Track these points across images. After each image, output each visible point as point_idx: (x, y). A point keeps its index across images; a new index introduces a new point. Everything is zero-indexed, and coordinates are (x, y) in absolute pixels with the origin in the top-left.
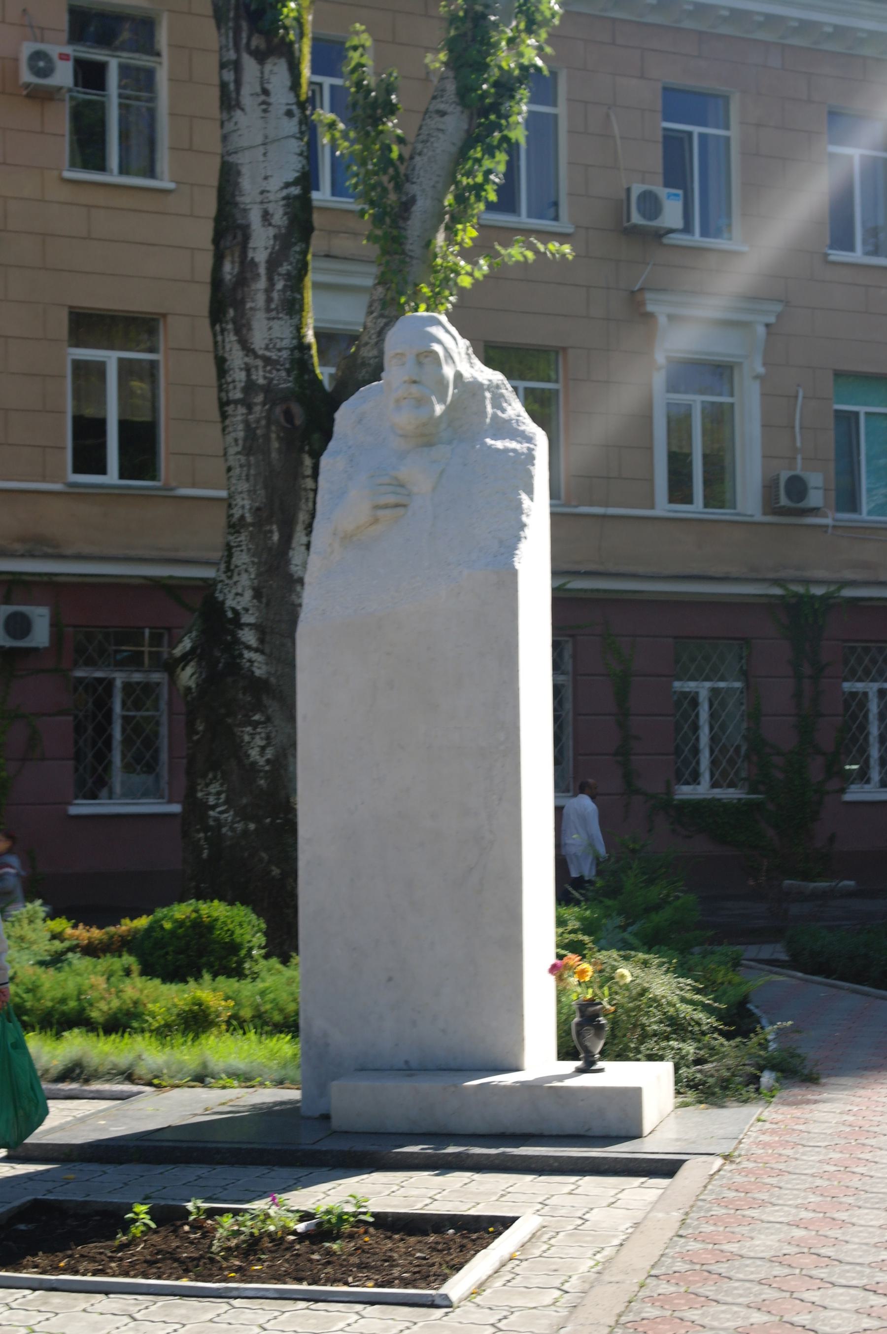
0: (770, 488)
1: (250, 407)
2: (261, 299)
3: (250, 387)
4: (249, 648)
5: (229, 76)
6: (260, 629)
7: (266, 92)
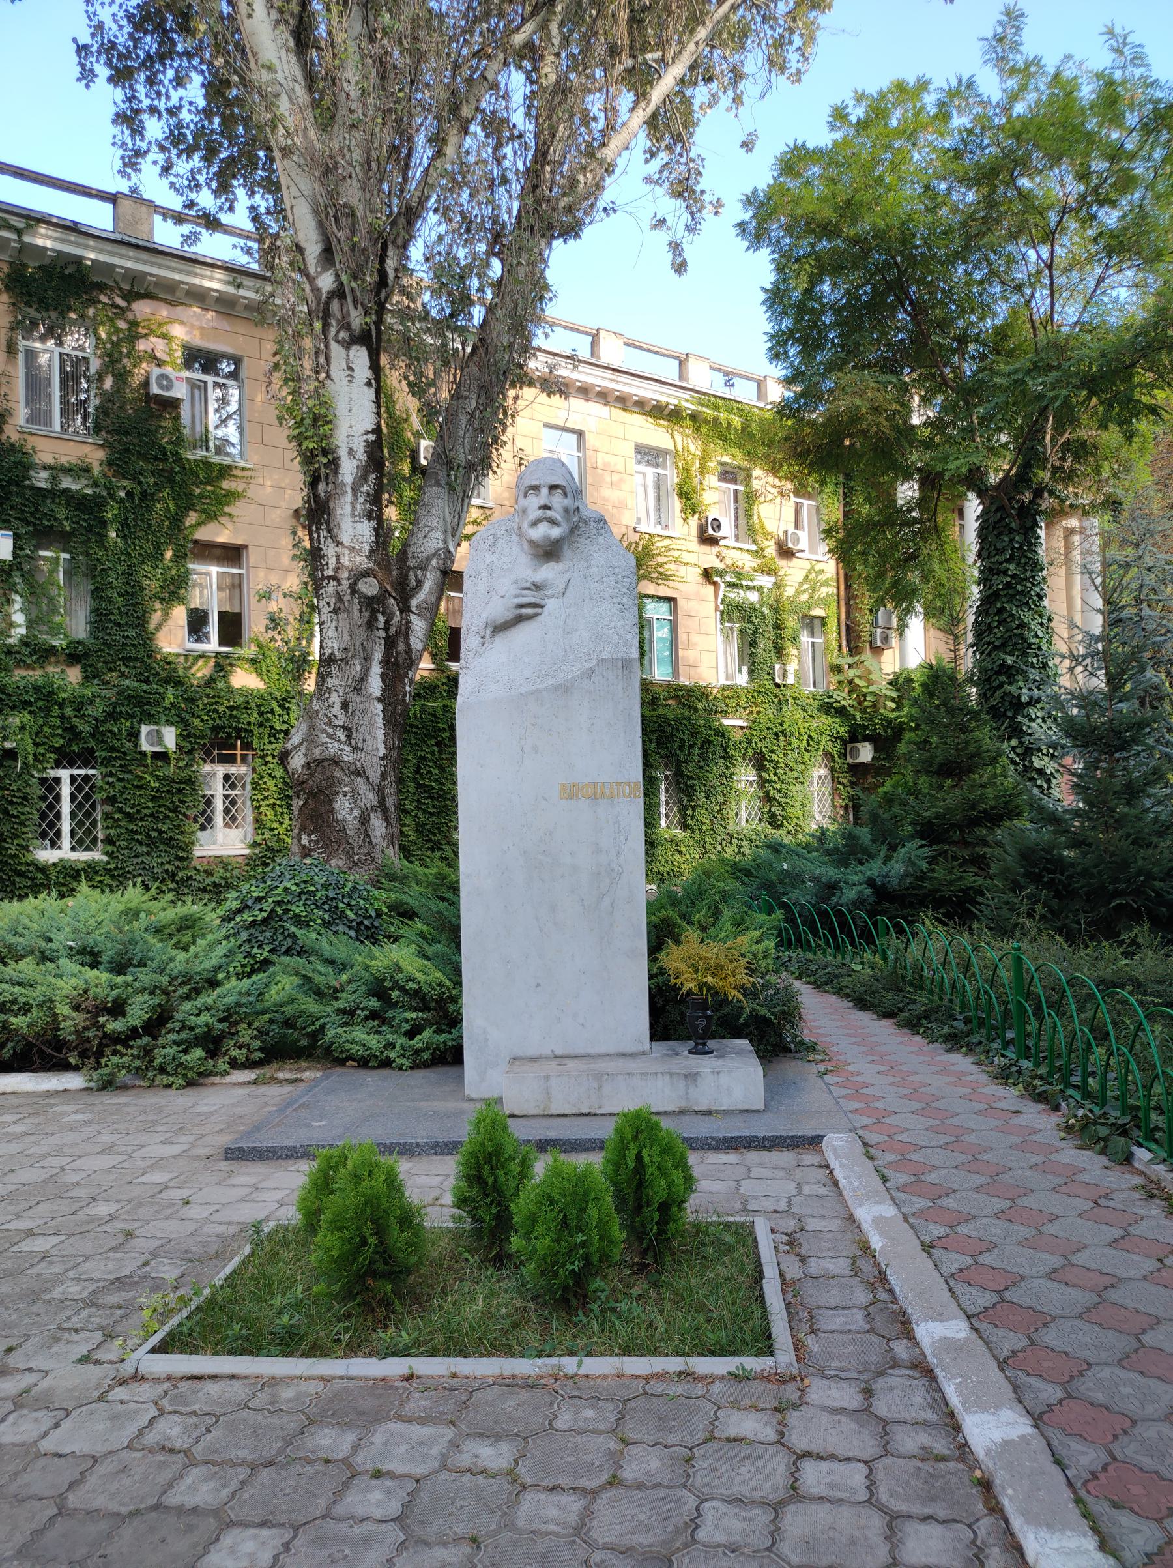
1: (338, 582)
7: (350, 368)
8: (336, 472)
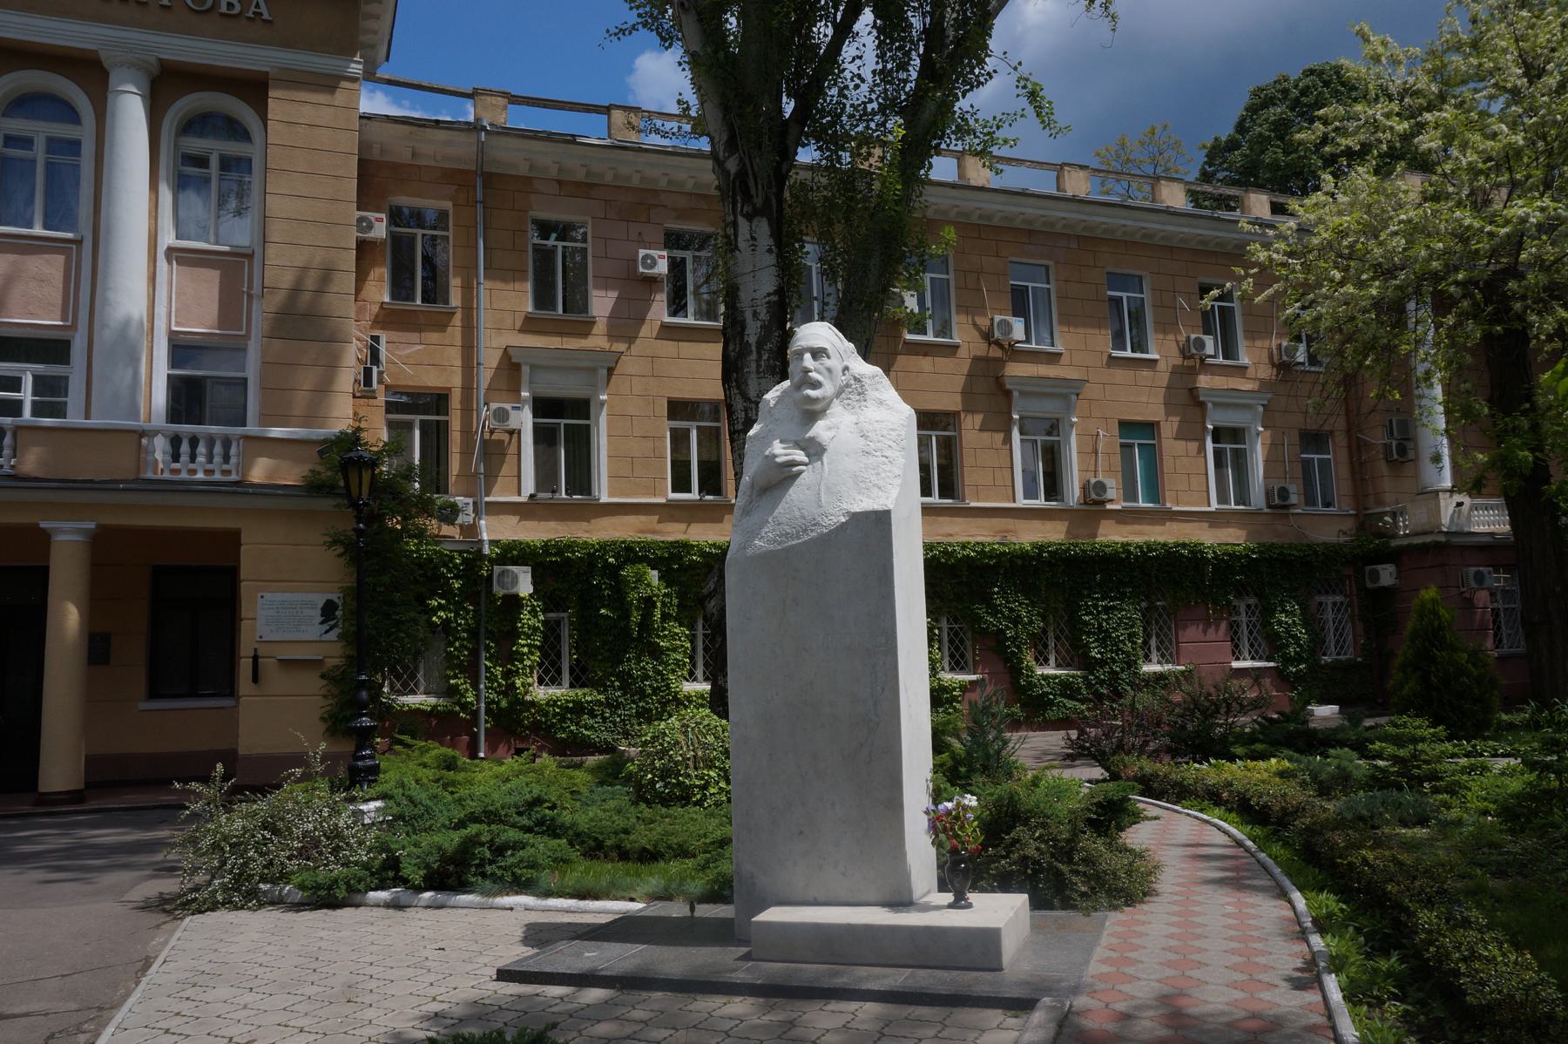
0: (1268, 494)
2: (753, 366)
5: (730, 231)
7: (753, 238)
8: (742, 333)
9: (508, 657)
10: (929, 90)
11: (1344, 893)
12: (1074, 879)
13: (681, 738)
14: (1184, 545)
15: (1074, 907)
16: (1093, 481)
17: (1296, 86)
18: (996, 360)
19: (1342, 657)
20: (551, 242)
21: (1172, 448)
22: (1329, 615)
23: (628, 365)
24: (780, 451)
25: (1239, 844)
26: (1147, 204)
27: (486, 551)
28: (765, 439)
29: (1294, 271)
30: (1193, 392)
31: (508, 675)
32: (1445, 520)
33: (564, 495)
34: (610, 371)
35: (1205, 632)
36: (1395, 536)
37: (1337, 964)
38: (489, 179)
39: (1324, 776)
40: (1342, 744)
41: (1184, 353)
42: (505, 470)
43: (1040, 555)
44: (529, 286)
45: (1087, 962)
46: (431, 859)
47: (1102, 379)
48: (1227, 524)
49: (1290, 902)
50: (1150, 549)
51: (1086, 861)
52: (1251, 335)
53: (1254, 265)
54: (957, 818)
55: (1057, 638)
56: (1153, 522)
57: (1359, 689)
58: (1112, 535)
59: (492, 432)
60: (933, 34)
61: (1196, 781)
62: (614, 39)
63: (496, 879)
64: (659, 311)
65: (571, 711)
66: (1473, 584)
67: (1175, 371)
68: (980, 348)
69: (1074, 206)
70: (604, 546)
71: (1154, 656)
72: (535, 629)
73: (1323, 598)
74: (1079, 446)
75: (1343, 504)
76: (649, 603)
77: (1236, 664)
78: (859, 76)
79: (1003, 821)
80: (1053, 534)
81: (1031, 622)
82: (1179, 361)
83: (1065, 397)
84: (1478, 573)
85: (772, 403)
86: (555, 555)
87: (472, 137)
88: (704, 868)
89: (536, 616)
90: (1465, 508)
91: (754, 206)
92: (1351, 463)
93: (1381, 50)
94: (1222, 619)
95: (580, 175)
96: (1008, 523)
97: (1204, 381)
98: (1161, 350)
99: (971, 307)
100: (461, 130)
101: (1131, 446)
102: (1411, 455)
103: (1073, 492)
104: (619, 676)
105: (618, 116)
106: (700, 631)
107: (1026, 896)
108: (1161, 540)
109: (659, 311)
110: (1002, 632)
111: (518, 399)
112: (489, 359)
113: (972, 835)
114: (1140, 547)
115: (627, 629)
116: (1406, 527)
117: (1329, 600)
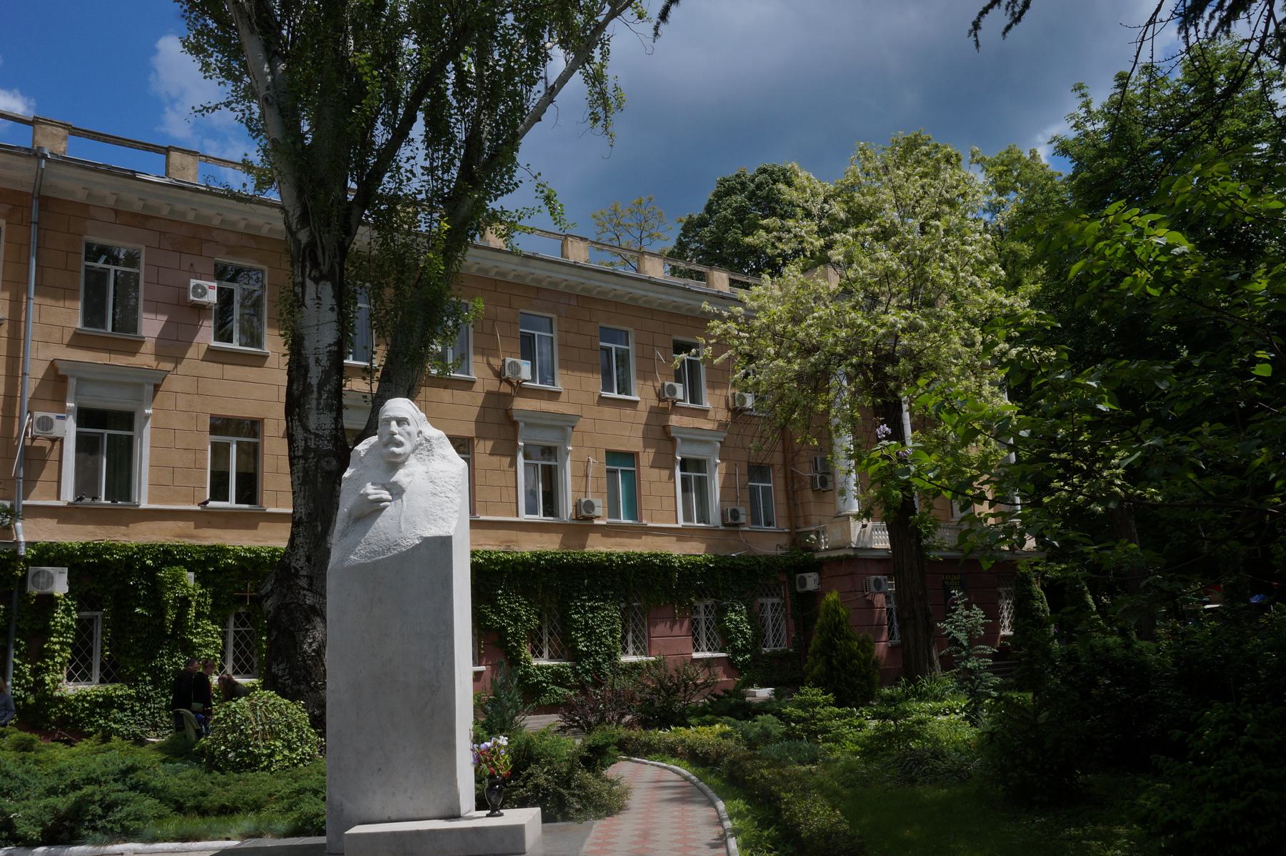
0: (723, 514)
1: (306, 460)
2: (314, 403)
3: (307, 449)
4: (304, 589)
5: (298, 290)
6: (310, 578)
7: (319, 298)
8: (305, 376)
9: (38, 655)
10: (468, 190)
11: (750, 799)
12: (573, 800)
13: (250, 715)
14: (656, 556)
15: (571, 819)
16: (584, 500)
17: (753, 181)
18: (506, 395)
19: (778, 649)
20: (100, 264)
21: (650, 475)
22: (769, 614)
23: (174, 383)
24: (371, 490)
25: (686, 779)
26: (632, 273)
27: (22, 552)
28: (358, 481)
29: (742, 343)
30: (666, 429)
31: (35, 672)
32: (854, 539)
33: (103, 501)
34: (157, 388)
35: (671, 628)
36: (818, 550)
37: (736, 832)
38: (46, 203)
39: (751, 735)
40: (767, 712)
41: (660, 396)
42: (45, 475)
43: (538, 562)
44: (79, 305)
45: (581, 846)
46: (47, 818)
47: (595, 416)
48: (691, 539)
49: (715, 807)
50: (629, 558)
51: (579, 787)
52: (713, 385)
53: (712, 337)
54: (494, 752)
55: (551, 634)
56: (632, 536)
57: (784, 675)
58: (598, 546)
59: (33, 439)
60: (473, 139)
61: (659, 741)
62: (199, 115)
63: (104, 830)
64: (206, 335)
65: (97, 704)
66: (874, 590)
67: (652, 411)
68: (493, 384)
69: (575, 271)
70: (142, 550)
71: (631, 649)
72: (68, 627)
73: (764, 600)
74: (573, 470)
75: (780, 524)
76: (184, 602)
77: (696, 655)
78: (411, 172)
79: (524, 757)
80: (549, 544)
81: (529, 620)
82: (655, 403)
83: (563, 429)
84: (876, 580)
85: (363, 454)
86: (93, 557)
87: (32, 163)
88: (290, 809)
89: (69, 615)
90: (868, 529)
91: (321, 272)
92: (787, 491)
93: (806, 183)
94: (685, 617)
95: (137, 207)
96: (503, 534)
97: (675, 420)
98: (642, 393)
99: (487, 350)
100: (21, 155)
101: (615, 472)
102: (830, 486)
103: (567, 509)
104: (151, 671)
105: (175, 157)
106: (231, 628)
107: (538, 809)
108: (638, 551)
109: (206, 335)
110: (504, 628)
111: (63, 408)
112: (35, 370)
113: (504, 763)
114: (621, 557)
115: (162, 626)
116: (826, 543)
117: (769, 601)
